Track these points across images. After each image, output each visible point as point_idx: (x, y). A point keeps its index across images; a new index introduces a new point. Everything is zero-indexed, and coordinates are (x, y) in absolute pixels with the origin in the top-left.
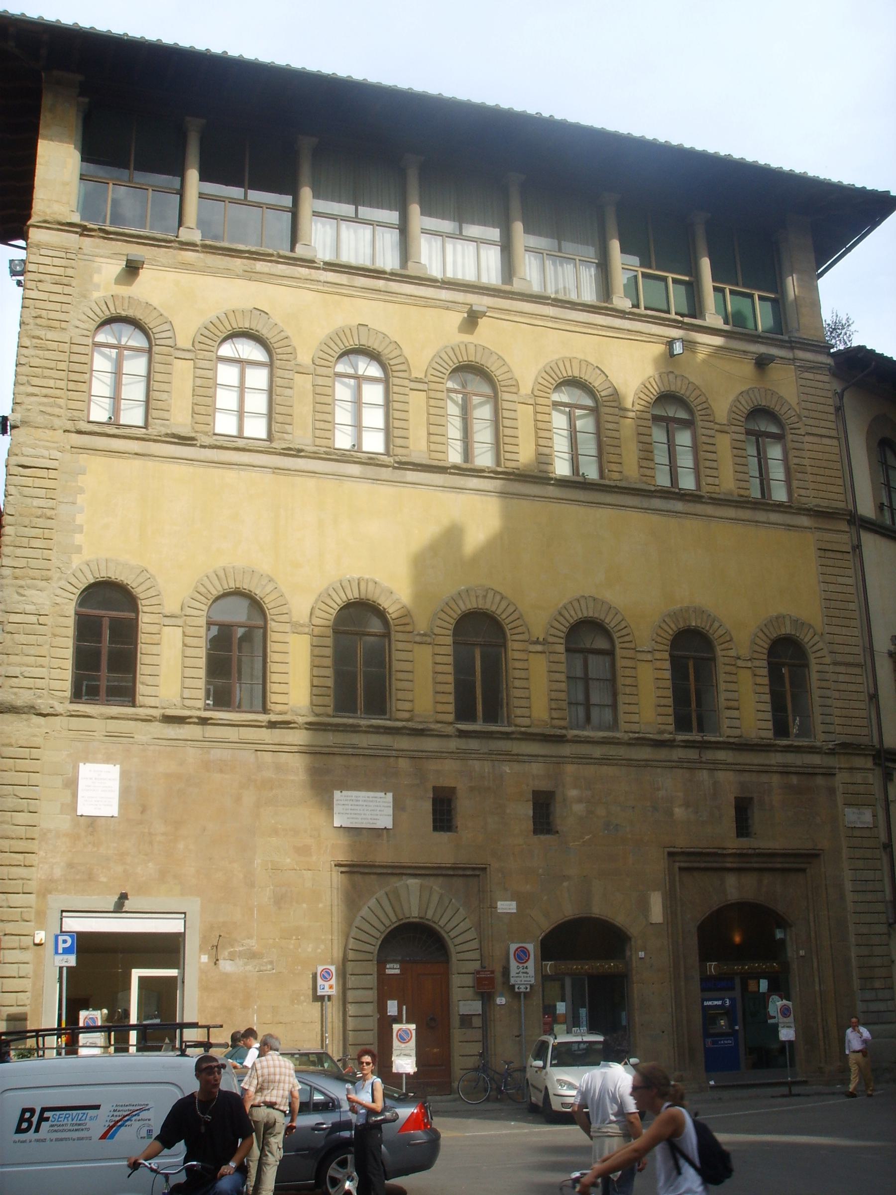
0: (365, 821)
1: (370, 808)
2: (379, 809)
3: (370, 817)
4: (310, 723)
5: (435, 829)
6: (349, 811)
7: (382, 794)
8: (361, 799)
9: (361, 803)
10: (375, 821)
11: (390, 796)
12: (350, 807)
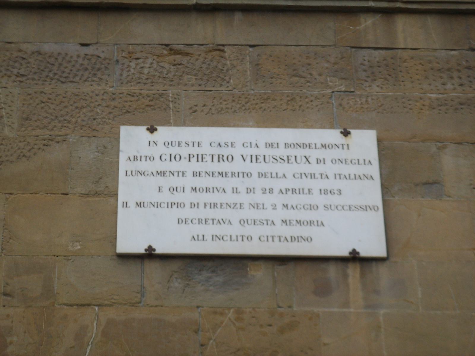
0: (255, 231)
1: (282, 184)
2: (317, 185)
3: (281, 214)
4: (207, 79)
5: (354, 250)
6: (188, 197)
7: (333, 136)
8: (237, 152)
9: (238, 166)
10: (304, 231)
11: (365, 142)
12: (189, 181)
